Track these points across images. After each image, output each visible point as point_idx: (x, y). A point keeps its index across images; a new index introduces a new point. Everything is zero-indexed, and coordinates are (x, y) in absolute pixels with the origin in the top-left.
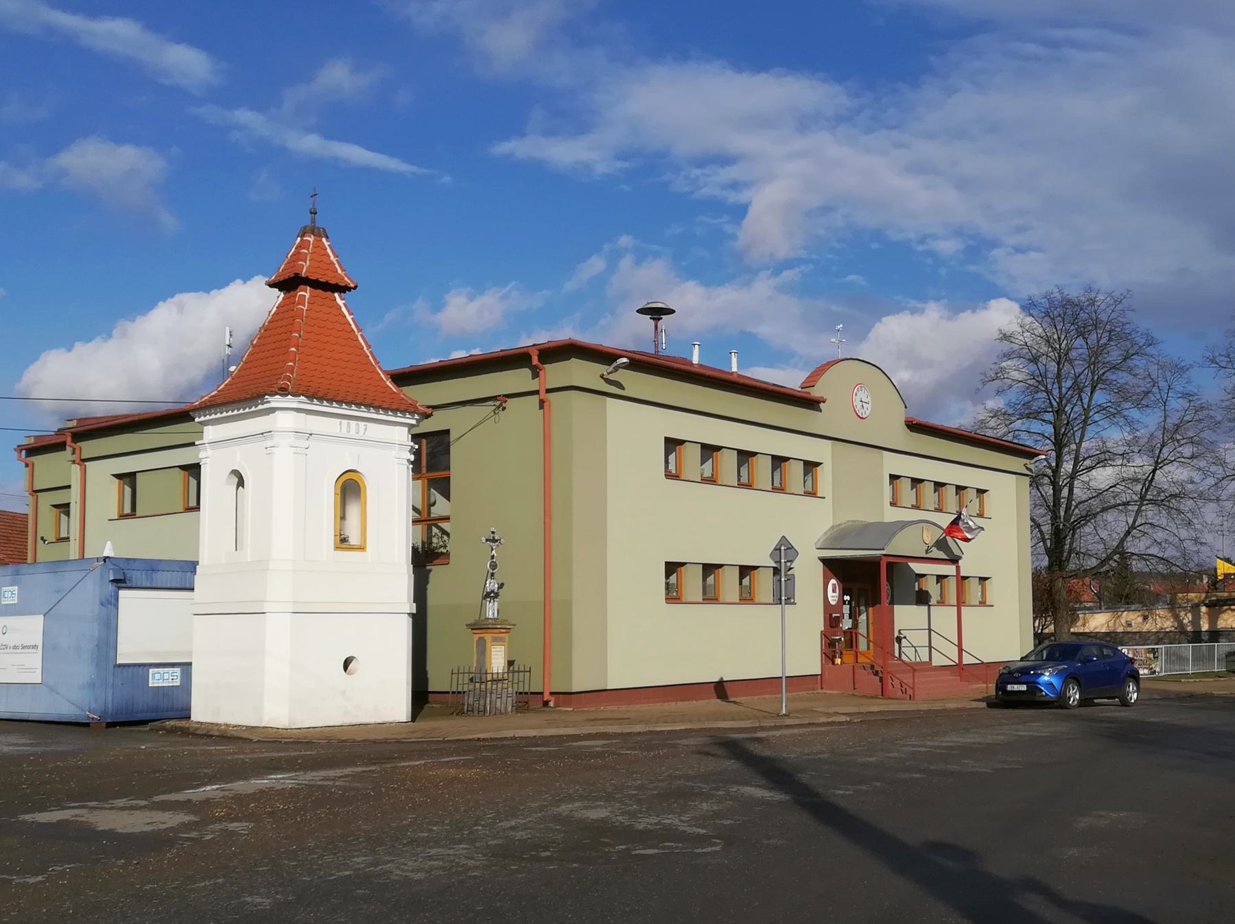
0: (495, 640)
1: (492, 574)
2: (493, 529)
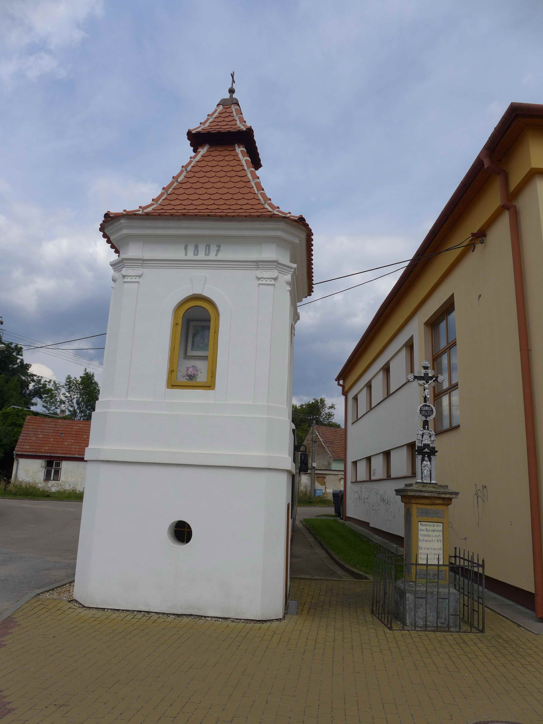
0: (426, 513)
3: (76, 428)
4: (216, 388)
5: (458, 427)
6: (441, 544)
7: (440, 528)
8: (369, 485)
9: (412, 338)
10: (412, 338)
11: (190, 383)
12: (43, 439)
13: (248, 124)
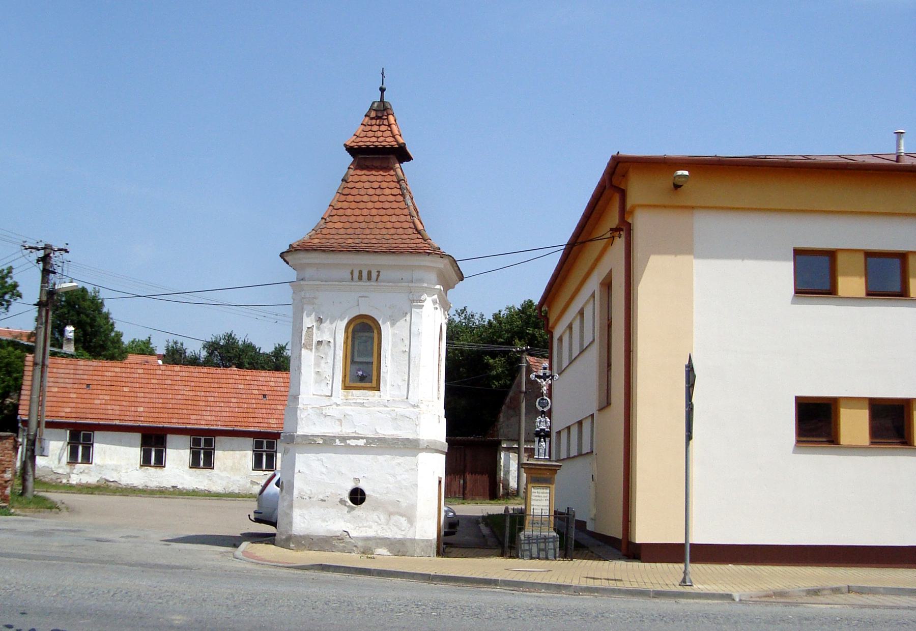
3: (110, 374)
4: (440, 559)
7: (548, 491)
8: (580, 459)
9: (610, 274)
10: (610, 274)
11: (332, 344)
12: (60, 395)
13: (401, 140)
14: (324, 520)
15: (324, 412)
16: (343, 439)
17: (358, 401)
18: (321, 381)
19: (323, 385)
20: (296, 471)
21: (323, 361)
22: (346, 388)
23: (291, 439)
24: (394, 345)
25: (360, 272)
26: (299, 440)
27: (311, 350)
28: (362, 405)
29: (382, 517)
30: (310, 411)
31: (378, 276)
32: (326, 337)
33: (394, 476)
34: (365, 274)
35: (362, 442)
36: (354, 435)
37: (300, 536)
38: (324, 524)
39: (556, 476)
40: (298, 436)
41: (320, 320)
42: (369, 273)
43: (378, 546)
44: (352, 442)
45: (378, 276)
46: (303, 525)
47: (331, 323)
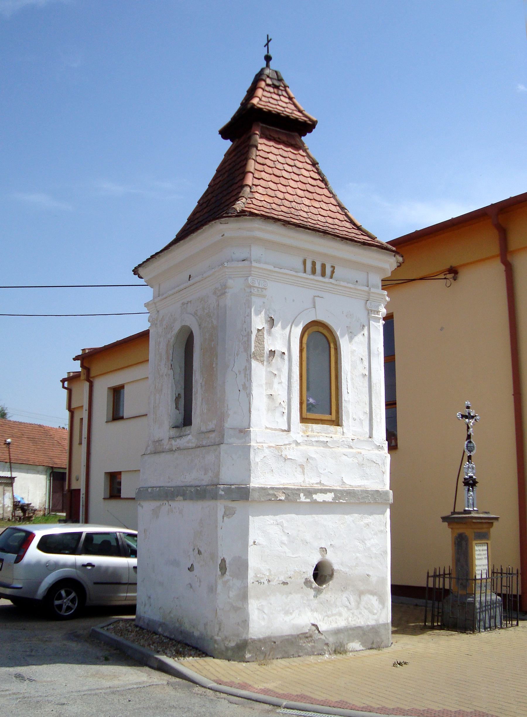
1: (470, 457)
2: (468, 403)
5: (75, 359)
6: (487, 561)
7: (486, 548)
11: (286, 357)
14: (287, 613)
15: (284, 454)
16: (309, 492)
17: (322, 439)
18: (275, 409)
19: (278, 414)
20: (251, 542)
21: (276, 380)
22: (303, 420)
23: (242, 493)
24: (354, 367)
25: (314, 264)
26: (254, 495)
27: (263, 364)
28: (325, 444)
29: (352, 599)
30: (266, 451)
31: (333, 272)
32: (279, 346)
33: (363, 541)
34: (318, 267)
35: (329, 497)
36: (319, 487)
37: (260, 640)
38: (287, 618)
39: (492, 530)
40: (254, 489)
41: (272, 322)
42: (323, 266)
43: (351, 639)
44: (319, 497)
45: (333, 272)
46: (263, 623)
47: (283, 328)
